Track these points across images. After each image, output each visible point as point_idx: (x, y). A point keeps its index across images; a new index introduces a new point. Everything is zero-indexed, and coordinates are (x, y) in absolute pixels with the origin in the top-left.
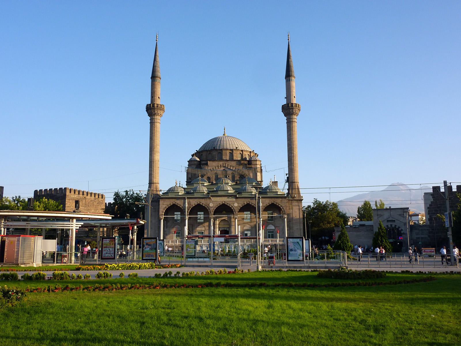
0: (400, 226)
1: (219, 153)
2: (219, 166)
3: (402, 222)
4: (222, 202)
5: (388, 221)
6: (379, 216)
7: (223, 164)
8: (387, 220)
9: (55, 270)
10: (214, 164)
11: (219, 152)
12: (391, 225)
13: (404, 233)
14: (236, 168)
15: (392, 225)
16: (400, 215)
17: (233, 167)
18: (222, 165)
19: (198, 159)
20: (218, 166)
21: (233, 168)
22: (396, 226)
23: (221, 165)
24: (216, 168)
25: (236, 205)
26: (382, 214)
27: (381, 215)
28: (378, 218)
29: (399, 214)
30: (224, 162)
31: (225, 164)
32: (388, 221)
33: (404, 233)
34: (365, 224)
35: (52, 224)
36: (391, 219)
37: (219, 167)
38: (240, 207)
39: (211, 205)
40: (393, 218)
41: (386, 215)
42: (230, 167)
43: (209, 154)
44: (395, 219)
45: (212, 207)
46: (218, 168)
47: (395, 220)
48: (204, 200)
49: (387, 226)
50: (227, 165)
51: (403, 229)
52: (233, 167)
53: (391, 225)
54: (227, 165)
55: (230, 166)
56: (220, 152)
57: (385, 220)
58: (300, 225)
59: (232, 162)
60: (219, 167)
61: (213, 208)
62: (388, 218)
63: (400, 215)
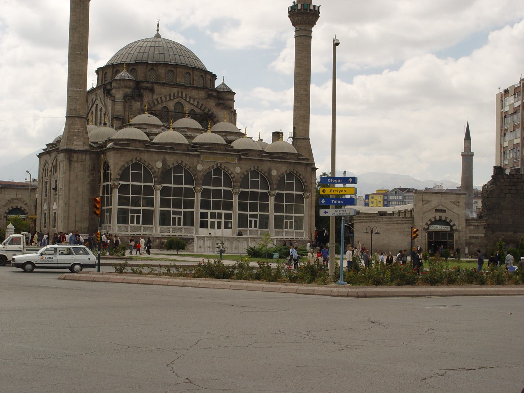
0: (452, 220)
1: (169, 70)
2: (172, 94)
3: (456, 213)
4: (217, 164)
5: (437, 211)
6: (424, 202)
7: (178, 92)
8: (436, 209)
9: (455, 260)
10: (163, 90)
11: (169, 69)
12: (440, 217)
13: (457, 229)
14: (198, 103)
15: (435, 217)
16: (454, 203)
17: (194, 100)
18: (176, 94)
19: (129, 75)
20: (170, 95)
21: (194, 101)
22: (446, 218)
23: (174, 94)
24: (166, 98)
25: (238, 170)
26: (429, 200)
27: (428, 202)
28: (423, 205)
29: (453, 201)
30: (180, 90)
31: (182, 92)
32: (437, 211)
33: (457, 229)
34: (387, 212)
35: (46, 191)
36: (440, 208)
37: (172, 98)
38: (243, 174)
39: (200, 167)
40: (445, 207)
41: (435, 202)
42: (190, 100)
43: (150, 69)
44: (446, 208)
45: (200, 171)
46: (170, 99)
47: (446, 210)
48: (188, 157)
49: (435, 218)
50: (184, 95)
51: (455, 223)
52: (194, 100)
53: (440, 217)
54: (184, 95)
55: (190, 98)
56: (173, 69)
57: (433, 209)
58: (311, 209)
59: (193, 91)
60: (172, 98)
61: (202, 174)
62: (437, 207)
63: (454, 203)
